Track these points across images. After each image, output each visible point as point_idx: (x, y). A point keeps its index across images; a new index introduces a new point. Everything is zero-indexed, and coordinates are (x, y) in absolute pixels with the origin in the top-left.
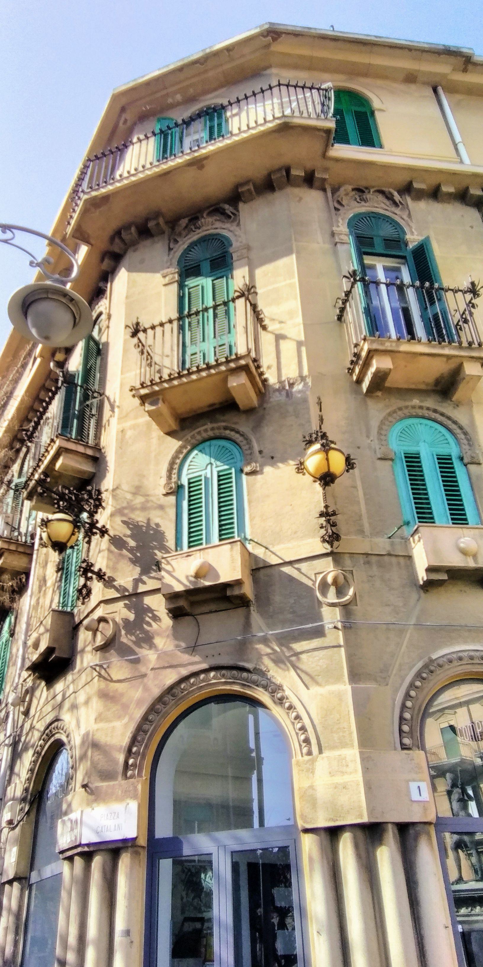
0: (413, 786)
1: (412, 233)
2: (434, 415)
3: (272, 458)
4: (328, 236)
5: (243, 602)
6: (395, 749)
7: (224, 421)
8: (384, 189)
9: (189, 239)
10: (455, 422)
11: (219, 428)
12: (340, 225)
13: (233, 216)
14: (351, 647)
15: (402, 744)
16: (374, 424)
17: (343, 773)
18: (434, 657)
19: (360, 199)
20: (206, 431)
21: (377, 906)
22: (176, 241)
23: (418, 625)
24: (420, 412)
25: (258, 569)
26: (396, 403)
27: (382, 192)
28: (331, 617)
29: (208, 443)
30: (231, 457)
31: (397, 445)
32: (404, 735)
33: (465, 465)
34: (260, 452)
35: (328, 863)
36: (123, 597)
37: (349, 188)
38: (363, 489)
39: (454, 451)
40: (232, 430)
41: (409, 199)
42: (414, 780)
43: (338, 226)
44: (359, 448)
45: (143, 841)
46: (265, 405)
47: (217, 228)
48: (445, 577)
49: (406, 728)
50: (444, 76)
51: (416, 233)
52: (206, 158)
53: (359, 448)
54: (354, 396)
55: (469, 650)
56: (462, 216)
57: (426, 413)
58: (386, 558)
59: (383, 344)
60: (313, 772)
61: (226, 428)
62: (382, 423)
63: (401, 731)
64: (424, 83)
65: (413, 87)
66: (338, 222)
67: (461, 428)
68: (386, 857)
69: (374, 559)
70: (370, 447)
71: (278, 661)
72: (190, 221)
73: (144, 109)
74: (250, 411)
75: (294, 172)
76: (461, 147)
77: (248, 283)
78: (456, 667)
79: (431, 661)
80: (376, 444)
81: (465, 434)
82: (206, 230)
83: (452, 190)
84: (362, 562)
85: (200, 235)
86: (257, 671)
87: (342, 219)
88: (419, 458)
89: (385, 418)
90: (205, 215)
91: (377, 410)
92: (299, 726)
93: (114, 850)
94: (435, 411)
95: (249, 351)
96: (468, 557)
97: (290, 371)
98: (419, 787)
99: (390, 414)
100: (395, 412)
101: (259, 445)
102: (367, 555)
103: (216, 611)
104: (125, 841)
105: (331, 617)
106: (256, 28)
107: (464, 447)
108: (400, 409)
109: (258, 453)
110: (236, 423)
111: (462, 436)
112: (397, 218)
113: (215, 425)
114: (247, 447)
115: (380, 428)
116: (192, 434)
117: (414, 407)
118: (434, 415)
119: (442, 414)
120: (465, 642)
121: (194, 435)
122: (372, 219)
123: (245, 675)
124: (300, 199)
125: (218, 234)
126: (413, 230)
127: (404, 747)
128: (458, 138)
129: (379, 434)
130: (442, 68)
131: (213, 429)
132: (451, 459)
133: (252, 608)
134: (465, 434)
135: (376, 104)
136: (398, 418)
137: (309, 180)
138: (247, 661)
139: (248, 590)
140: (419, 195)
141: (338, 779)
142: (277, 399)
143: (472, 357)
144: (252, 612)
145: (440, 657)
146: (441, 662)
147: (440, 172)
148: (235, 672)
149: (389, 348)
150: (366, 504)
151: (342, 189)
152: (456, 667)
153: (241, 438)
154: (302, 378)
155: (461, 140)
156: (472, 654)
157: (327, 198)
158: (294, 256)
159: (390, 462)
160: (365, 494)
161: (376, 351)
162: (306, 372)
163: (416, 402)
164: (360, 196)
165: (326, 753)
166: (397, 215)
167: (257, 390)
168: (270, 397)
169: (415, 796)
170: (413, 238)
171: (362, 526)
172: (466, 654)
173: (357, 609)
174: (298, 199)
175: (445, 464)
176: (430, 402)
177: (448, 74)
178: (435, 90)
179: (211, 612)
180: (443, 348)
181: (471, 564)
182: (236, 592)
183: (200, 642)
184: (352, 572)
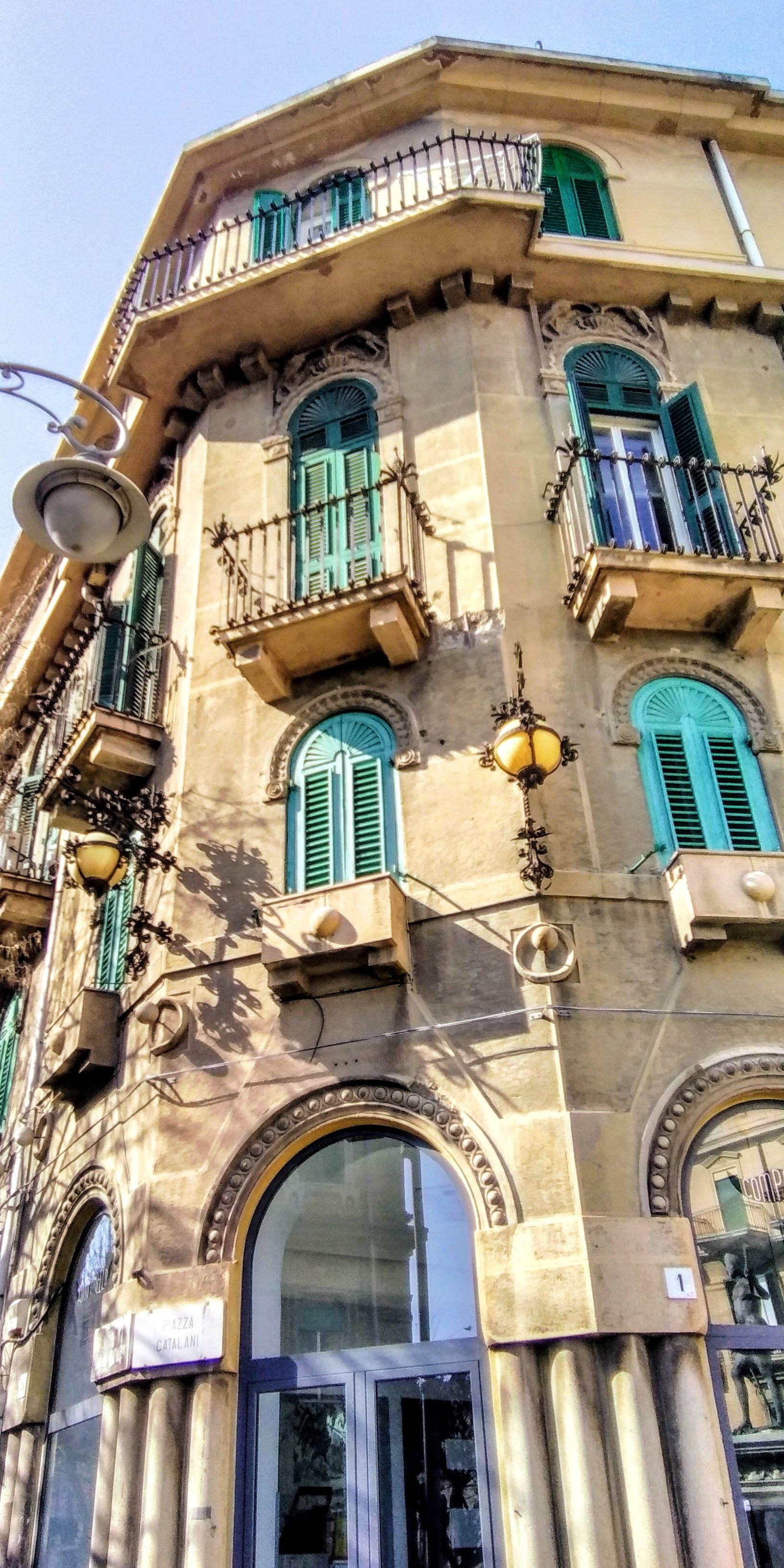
0: (671, 1274)
2: (703, 673)
3: (442, 742)
4: (532, 383)
5: (394, 976)
7: (363, 683)
8: (623, 306)
9: (307, 387)
10: (738, 685)
11: (355, 694)
12: (551, 364)
14: (570, 1049)
15: (652, 1206)
16: (608, 687)
18: (704, 1065)
19: (585, 323)
20: (334, 698)
22: (286, 391)
24: (682, 668)
25: (419, 923)
26: (643, 653)
28: (537, 1000)
29: (337, 719)
30: (376, 741)
31: (644, 721)
32: (656, 1191)
33: (756, 754)
34: (423, 733)
35: (533, 1399)
36: (201, 969)
37: (567, 304)
38: (590, 792)
39: (737, 731)
40: (377, 697)
42: (672, 1265)
43: (549, 367)
44: (582, 726)
45: (231, 1364)
46: (430, 657)
48: (722, 935)
49: (659, 1181)
50: (721, 123)
51: (675, 378)
53: (582, 726)
54: (574, 642)
55: (761, 1055)
56: (751, 350)
57: (691, 669)
61: (366, 694)
62: (620, 686)
63: (650, 1185)
64: (689, 135)
65: (670, 140)
67: (748, 694)
68: (626, 1388)
69: (607, 906)
70: (600, 725)
71: (451, 1072)
73: (233, 176)
74: (406, 667)
76: (748, 239)
77: (402, 459)
78: (740, 1081)
79: (700, 1072)
80: (610, 721)
81: (755, 703)
83: (733, 308)
84: (587, 911)
85: (325, 381)
86: (417, 1088)
87: (556, 356)
88: (679, 742)
89: (625, 678)
93: (185, 1379)
94: (706, 666)
95: (404, 569)
97: (471, 602)
98: (680, 1276)
100: (640, 668)
102: (596, 899)
103: (351, 991)
104: (202, 1363)
105: (537, 1000)
106: (416, 45)
108: (650, 663)
109: (418, 734)
110: (383, 686)
111: (751, 708)
113: (349, 689)
114: (401, 725)
115: (617, 694)
116: (311, 703)
117: (671, 660)
118: (703, 673)
119: (718, 672)
121: (314, 705)
123: (397, 1094)
124: (488, 323)
125: (354, 380)
126: (671, 373)
127: (656, 1211)
128: (743, 224)
129: (616, 703)
130: (717, 111)
131: (345, 696)
132: (731, 745)
133: (409, 986)
134: (755, 703)
135: (610, 168)
136: (646, 677)
137: (502, 292)
138: (402, 1072)
139: (402, 956)
140: (680, 317)
141: (551, 1264)
142: (449, 647)
143: (766, 580)
144: (409, 992)
146: (715, 1073)
149: (632, 565)
150: (595, 817)
151: (555, 307)
152: (740, 1081)
153: (391, 711)
154: (491, 613)
155: (748, 227)
156: (766, 1060)
157: (530, 321)
158: (477, 415)
159: (633, 750)
160: (592, 801)
162: (496, 604)
163: (675, 651)
164: (584, 318)
165: (530, 1221)
166: (645, 348)
167: (417, 632)
168: (438, 645)
169: (674, 1291)
171: (587, 852)
172: (756, 1060)
173: (580, 988)
174: (484, 322)
175: (722, 751)
176: (698, 652)
177: (727, 120)
179: (342, 992)
180: (719, 563)
181: (764, 914)
182: (383, 960)
183: (324, 1041)
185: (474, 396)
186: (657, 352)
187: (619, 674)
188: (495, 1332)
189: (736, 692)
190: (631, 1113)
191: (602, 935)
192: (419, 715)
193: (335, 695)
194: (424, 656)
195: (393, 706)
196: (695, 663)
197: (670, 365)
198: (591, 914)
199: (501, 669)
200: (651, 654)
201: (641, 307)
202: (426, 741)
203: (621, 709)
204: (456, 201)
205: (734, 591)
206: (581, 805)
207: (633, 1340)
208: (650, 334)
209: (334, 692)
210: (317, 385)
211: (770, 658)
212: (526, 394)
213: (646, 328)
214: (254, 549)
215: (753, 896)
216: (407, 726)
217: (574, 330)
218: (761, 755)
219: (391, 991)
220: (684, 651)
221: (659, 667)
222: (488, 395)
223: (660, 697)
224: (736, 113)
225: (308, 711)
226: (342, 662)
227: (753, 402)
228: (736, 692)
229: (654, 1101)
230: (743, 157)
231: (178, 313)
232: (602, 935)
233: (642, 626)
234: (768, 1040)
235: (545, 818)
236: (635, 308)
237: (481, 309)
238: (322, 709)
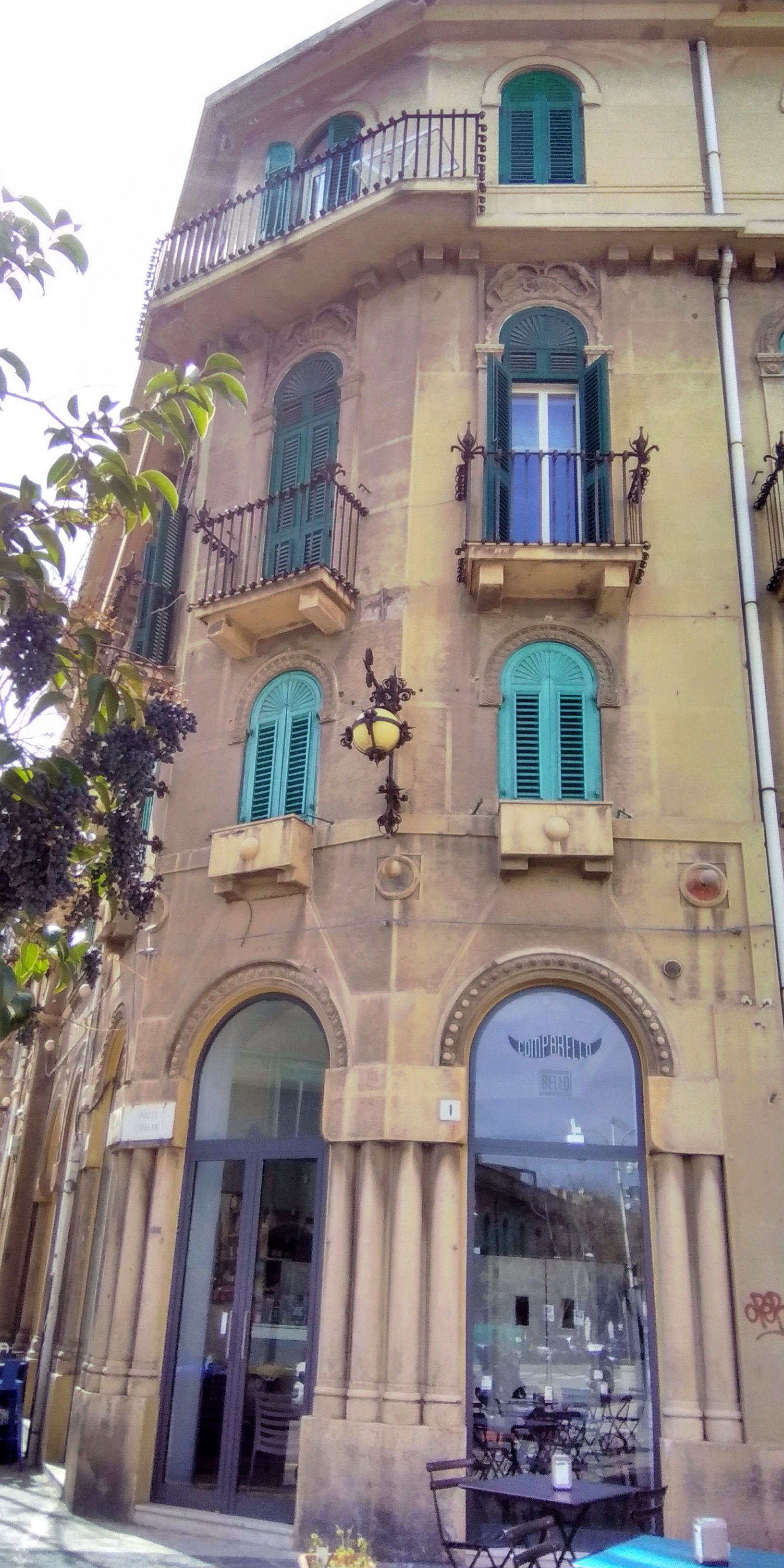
0: (445, 1105)
1: (596, 339)
2: (570, 638)
3: (353, 703)
4: (468, 356)
5: (298, 889)
6: (432, 1065)
7: (305, 648)
8: (566, 263)
9: (291, 360)
10: (596, 647)
11: (298, 657)
12: (487, 337)
13: (348, 323)
15: (441, 1058)
16: (484, 655)
17: (372, 1088)
18: (500, 961)
19: (528, 286)
20: (284, 659)
21: (388, 1224)
22: (277, 362)
23: (489, 925)
24: (552, 634)
25: (321, 848)
26: (522, 622)
27: (563, 268)
29: (285, 677)
30: (310, 698)
31: (511, 685)
32: (447, 1049)
33: (599, 709)
34: (341, 694)
35: (348, 1177)
37: (514, 267)
38: (453, 749)
39: (586, 688)
40: (313, 660)
41: (603, 277)
42: (447, 1098)
43: (485, 341)
44: (458, 691)
45: (181, 1142)
46: (353, 628)
47: (326, 344)
48: (524, 866)
49: (449, 1042)
50: (709, 23)
51: (601, 340)
52: (304, 244)
53: (458, 691)
54: (464, 615)
55: (545, 954)
56: (685, 297)
57: (561, 635)
58: (466, 838)
59: (491, 551)
60: (343, 1085)
61: (307, 657)
62: (495, 653)
63: (443, 1044)
64: (679, 37)
65: (657, 46)
66: (486, 332)
67: (604, 656)
69: (450, 840)
70: (472, 690)
72: (295, 328)
73: (251, 123)
74: (336, 635)
75: (427, 256)
76: (714, 161)
78: (526, 973)
79: (495, 965)
80: (480, 687)
81: (608, 663)
82: (313, 347)
83: (668, 256)
84: (434, 844)
85: (306, 354)
87: (493, 327)
88: (536, 701)
89: (500, 647)
90: (313, 321)
91: (492, 632)
92: (339, 1033)
93: (154, 1150)
94: (573, 632)
96: (555, 843)
98: (451, 1106)
99: (508, 640)
100: (516, 636)
101: (340, 685)
102: (441, 835)
103: (271, 897)
104: (161, 1141)
107: (602, 682)
108: (524, 631)
109: (337, 695)
110: (318, 652)
111: (603, 667)
112: (578, 315)
113: (295, 653)
114: (328, 685)
115: (491, 661)
116: (267, 663)
117: (543, 628)
118: (570, 638)
119: (583, 637)
120: (543, 944)
121: (270, 665)
122: (539, 317)
123: (293, 973)
124: (439, 294)
125: (328, 354)
126: (599, 335)
127: (443, 1062)
128: (713, 144)
129: (489, 669)
131: (292, 657)
132: (579, 701)
133: (308, 896)
134: (608, 663)
135: (589, 94)
136: (520, 643)
137: (451, 261)
138: (296, 958)
139: (302, 874)
140: (618, 269)
141: (368, 1094)
142: (368, 619)
143: (616, 561)
144: (308, 901)
145: (508, 962)
146: (506, 967)
147: (648, 231)
148: (282, 969)
149: (499, 557)
150: (454, 769)
151: (501, 272)
152: (526, 973)
153: (322, 673)
155: (716, 150)
156: (548, 958)
157: (477, 287)
159: (497, 710)
160: (454, 755)
161: (482, 561)
163: (549, 619)
164: (528, 280)
166: (582, 307)
167: (343, 607)
168: (360, 617)
169: (444, 1115)
170: (594, 348)
171: (443, 797)
172: (540, 958)
174: (435, 294)
175: (570, 708)
176: (567, 620)
177: (713, 21)
178: (694, 48)
179: (265, 898)
180: (575, 550)
181: (557, 851)
182: (287, 878)
183: (252, 932)
184: (419, 858)
185: (415, 376)
186: (590, 312)
187: (495, 643)
188: (329, 1135)
189: (593, 653)
190: (438, 995)
191: (442, 863)
192: (339, 679)
193: (286, 656)
194: (348, 628)
195: (324, 669)
196: (563, 629)
197: (600, 324)
198: (437, 847)
199: (400, 643)
200: (526, 622)
201: (582, 264)
202: (342, 701)
203: (493, 674)
204: (390, 196)
205: (592, 571)
206: (444, 759)
207: (411, 1148)
208: (589, 290)
209: (284, 654)
210: (298, 359)
211: (631, 618)
212: (462, 369)
213: (585, 284)
214: (604, 216)
215: (551, 838)
216: (331, 687)
217: (520, 294)
218: (602, 710)
219: (296, 900)
220: (556, 617)
221: (533, 634)
222: (427, 374)
223: (528, 661)
224: (723, 10)
225: (253, 682)
226: (291, 629)
227: (675, 357)
228: (593, 653)
229: (456, 986)
230: (735, 52)
231: (182, 299)
232: (442, 863)
233: (523, 596)
234: (553, 943)
235: (414, 770)
236: (576, 265)
237: (434, 280)
238: (276, 668)
